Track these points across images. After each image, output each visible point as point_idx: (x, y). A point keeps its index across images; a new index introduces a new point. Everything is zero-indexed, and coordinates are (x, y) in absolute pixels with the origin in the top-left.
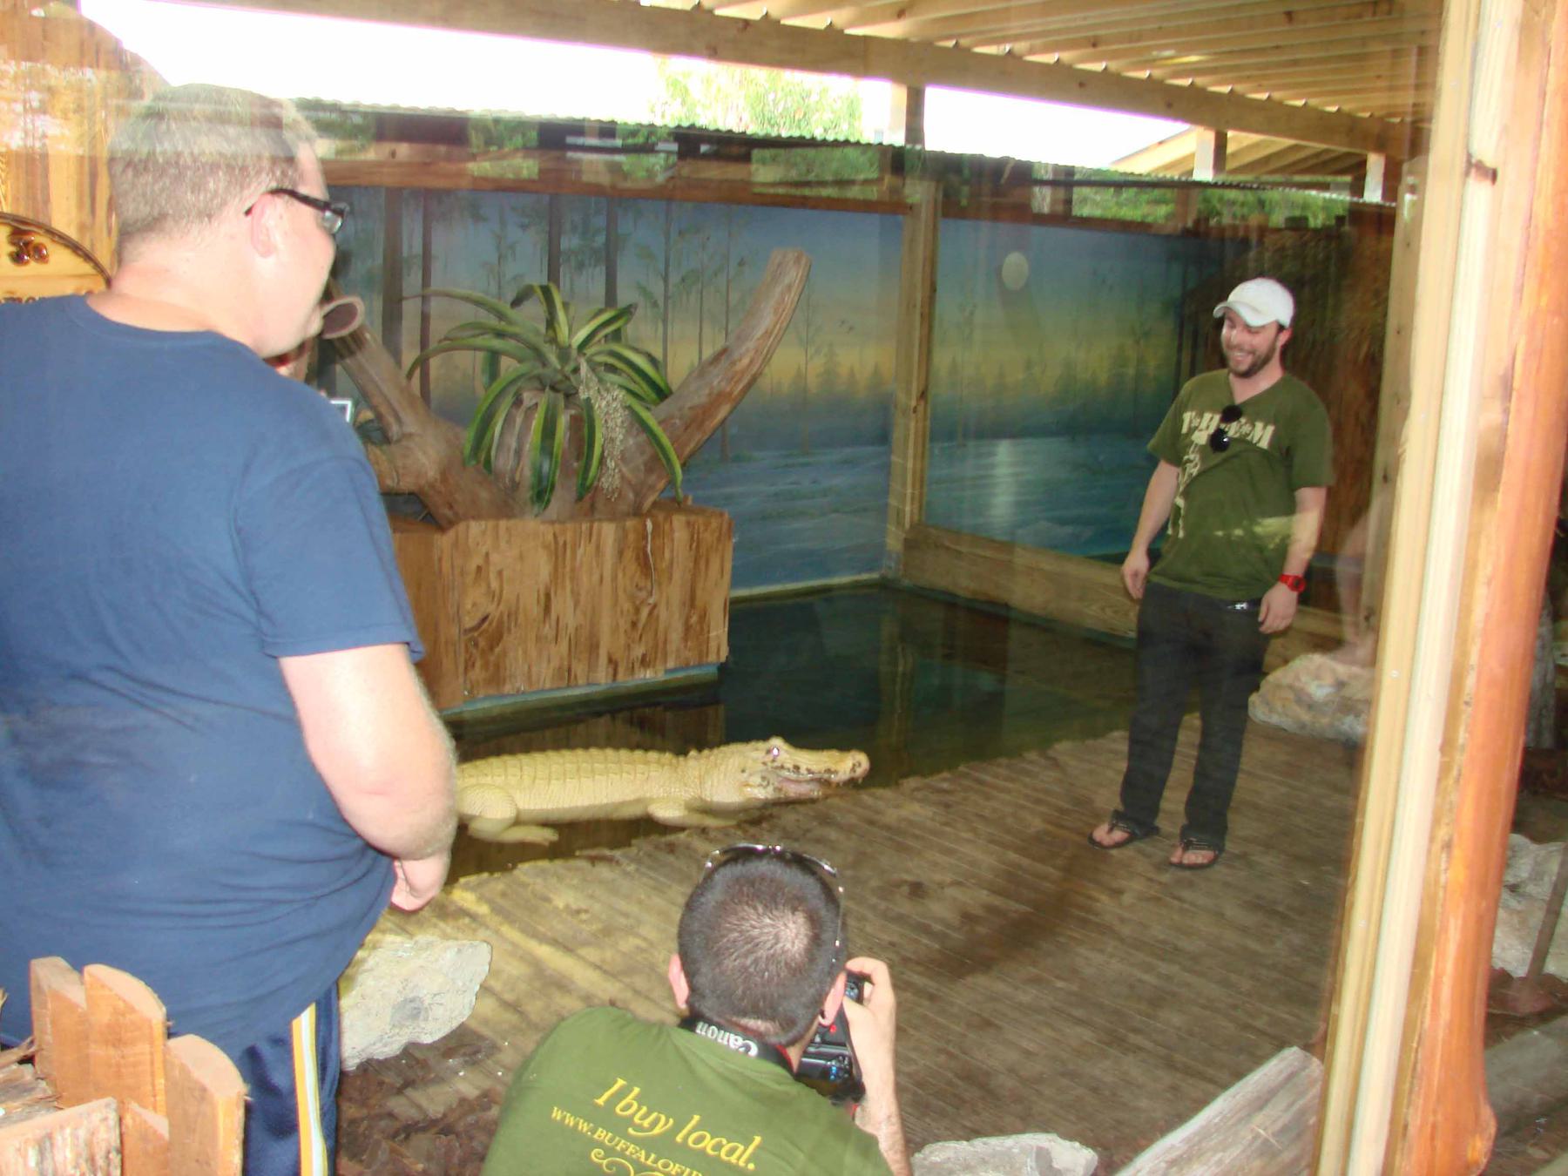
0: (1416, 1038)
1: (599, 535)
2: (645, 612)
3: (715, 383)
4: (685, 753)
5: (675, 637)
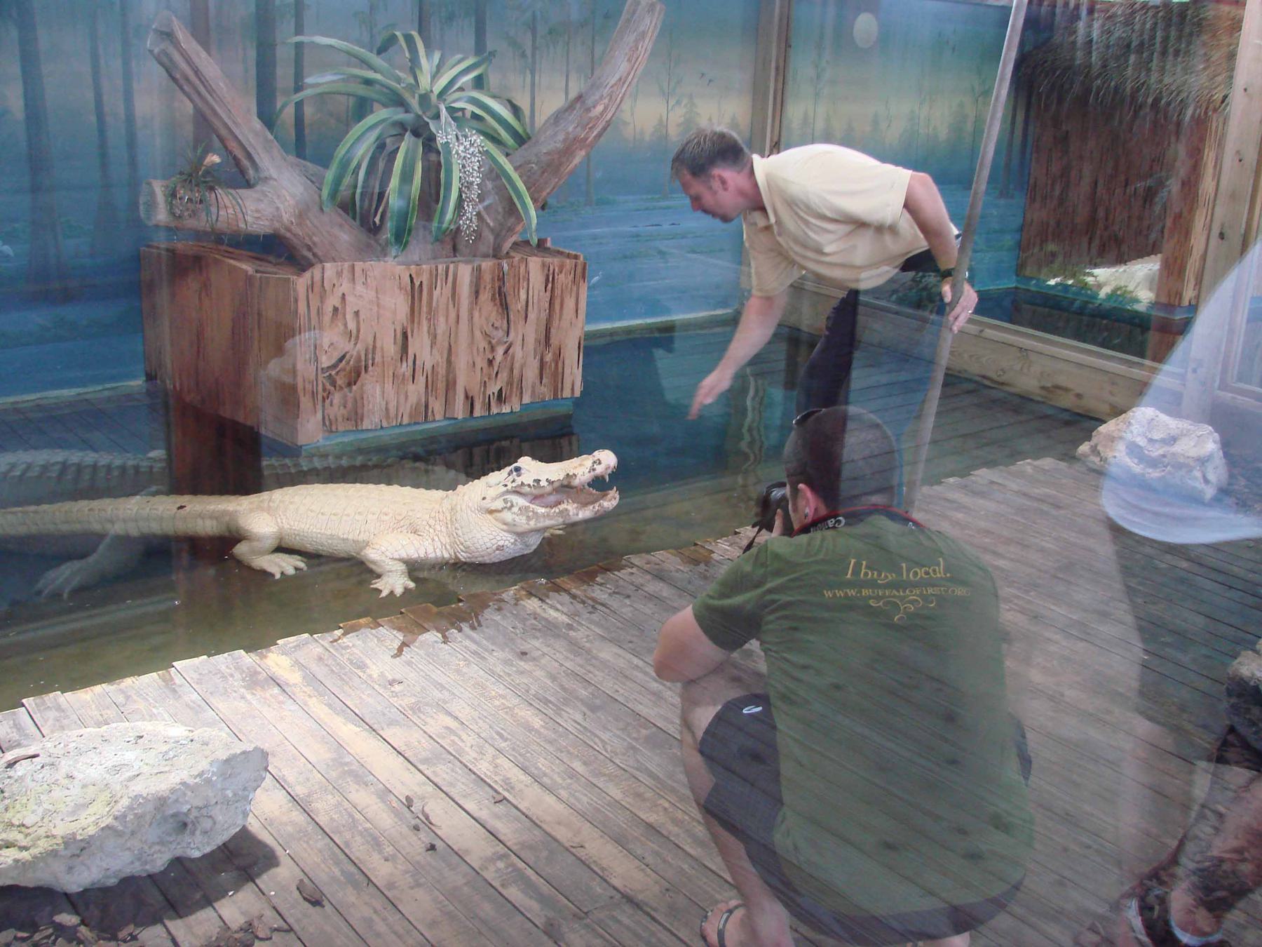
2: (500, 351)
3: (571, 129)
5: (531, 373)
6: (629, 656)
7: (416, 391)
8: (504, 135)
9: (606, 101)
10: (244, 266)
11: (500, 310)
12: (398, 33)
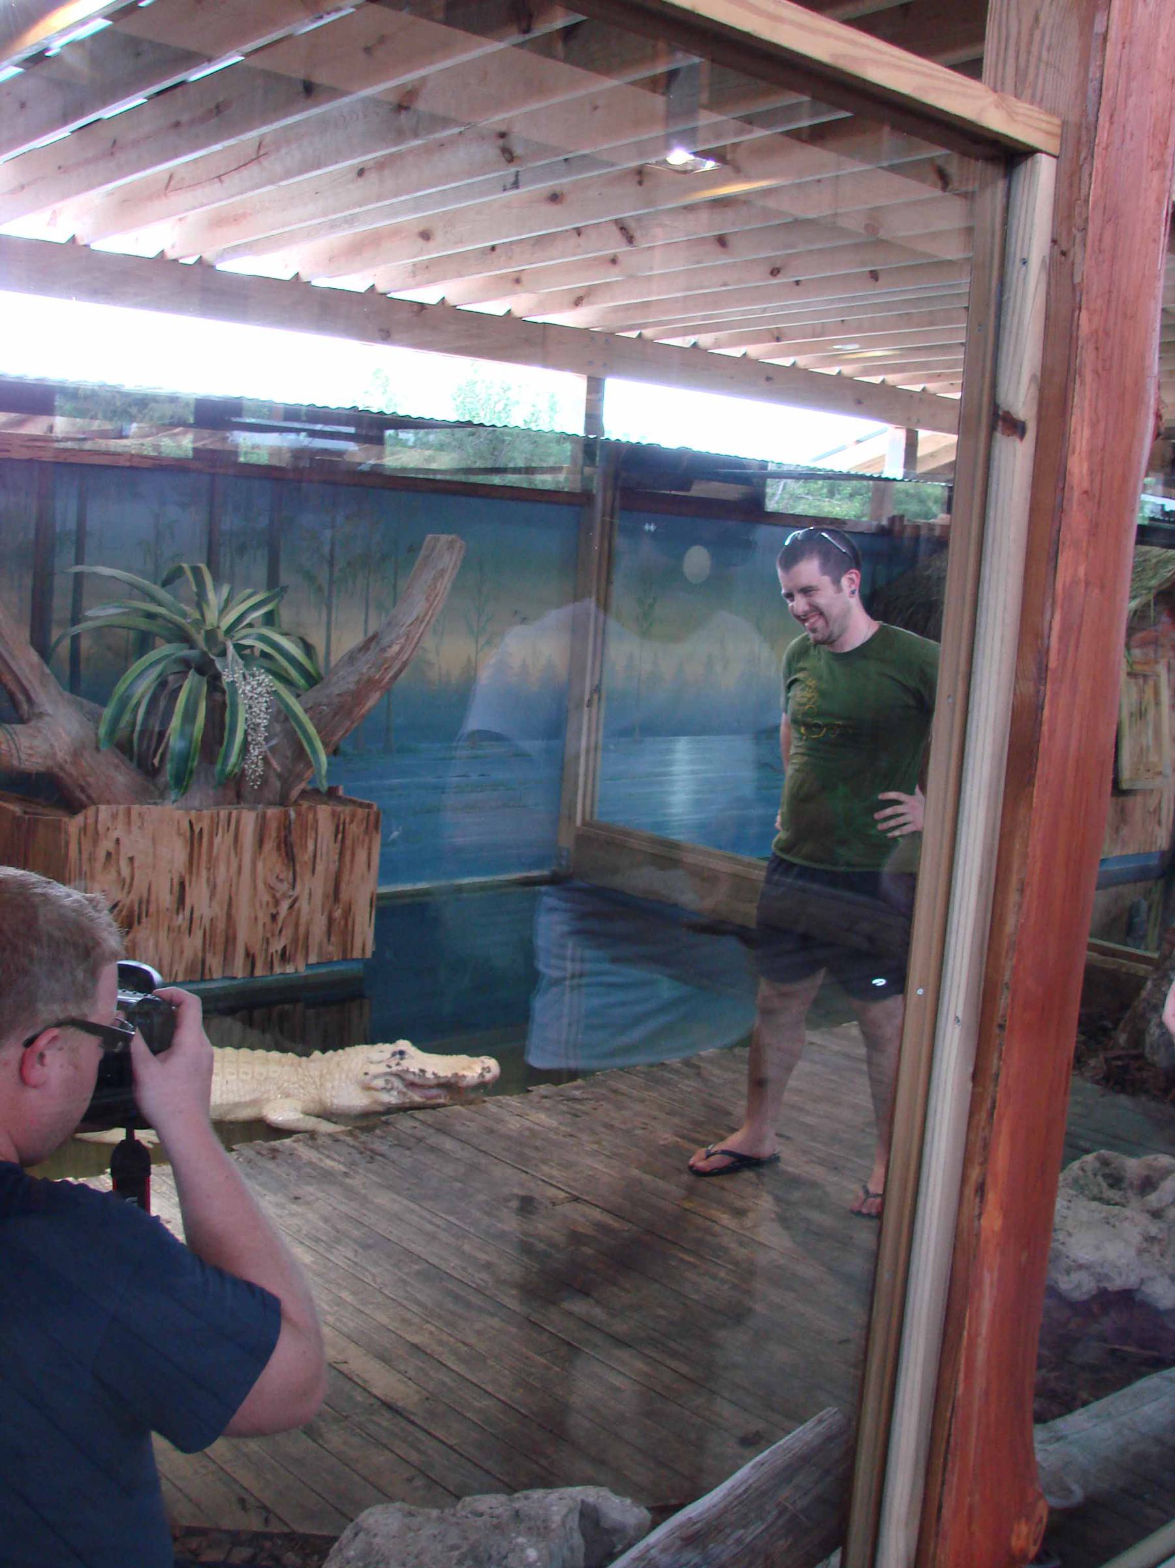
0: (950, 1408)
1: (238, 822)
2: (285, 905)
3: (365, 670)
4: (308, 1055)
6: (406, 1202)
7: (193, 944)
8: (294, 674)
9: (402, 641)
10: (11, 807)
11: (286, 862)
12: (185, 566)
